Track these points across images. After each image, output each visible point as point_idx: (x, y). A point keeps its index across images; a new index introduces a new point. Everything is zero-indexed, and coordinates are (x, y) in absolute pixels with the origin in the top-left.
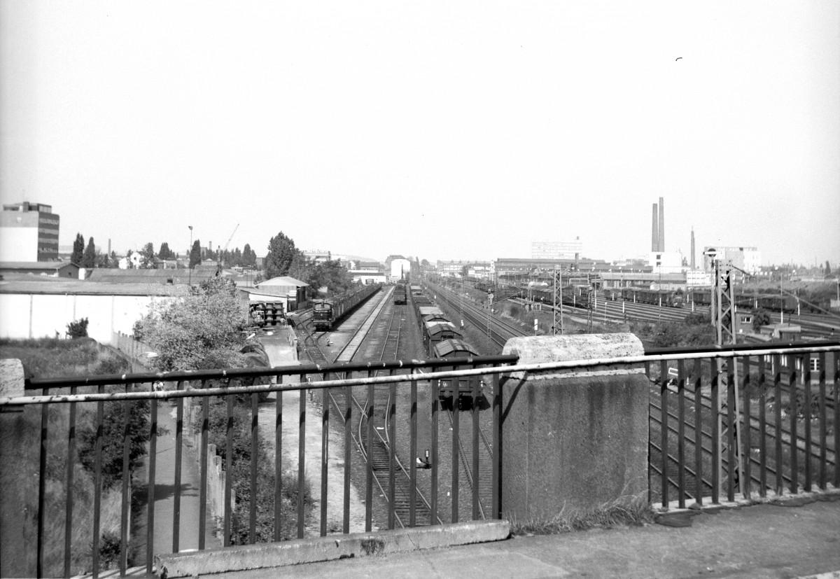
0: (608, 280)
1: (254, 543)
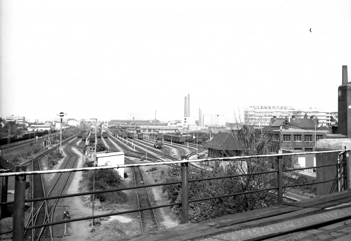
0: (143, 129)
1: (153, 194)
